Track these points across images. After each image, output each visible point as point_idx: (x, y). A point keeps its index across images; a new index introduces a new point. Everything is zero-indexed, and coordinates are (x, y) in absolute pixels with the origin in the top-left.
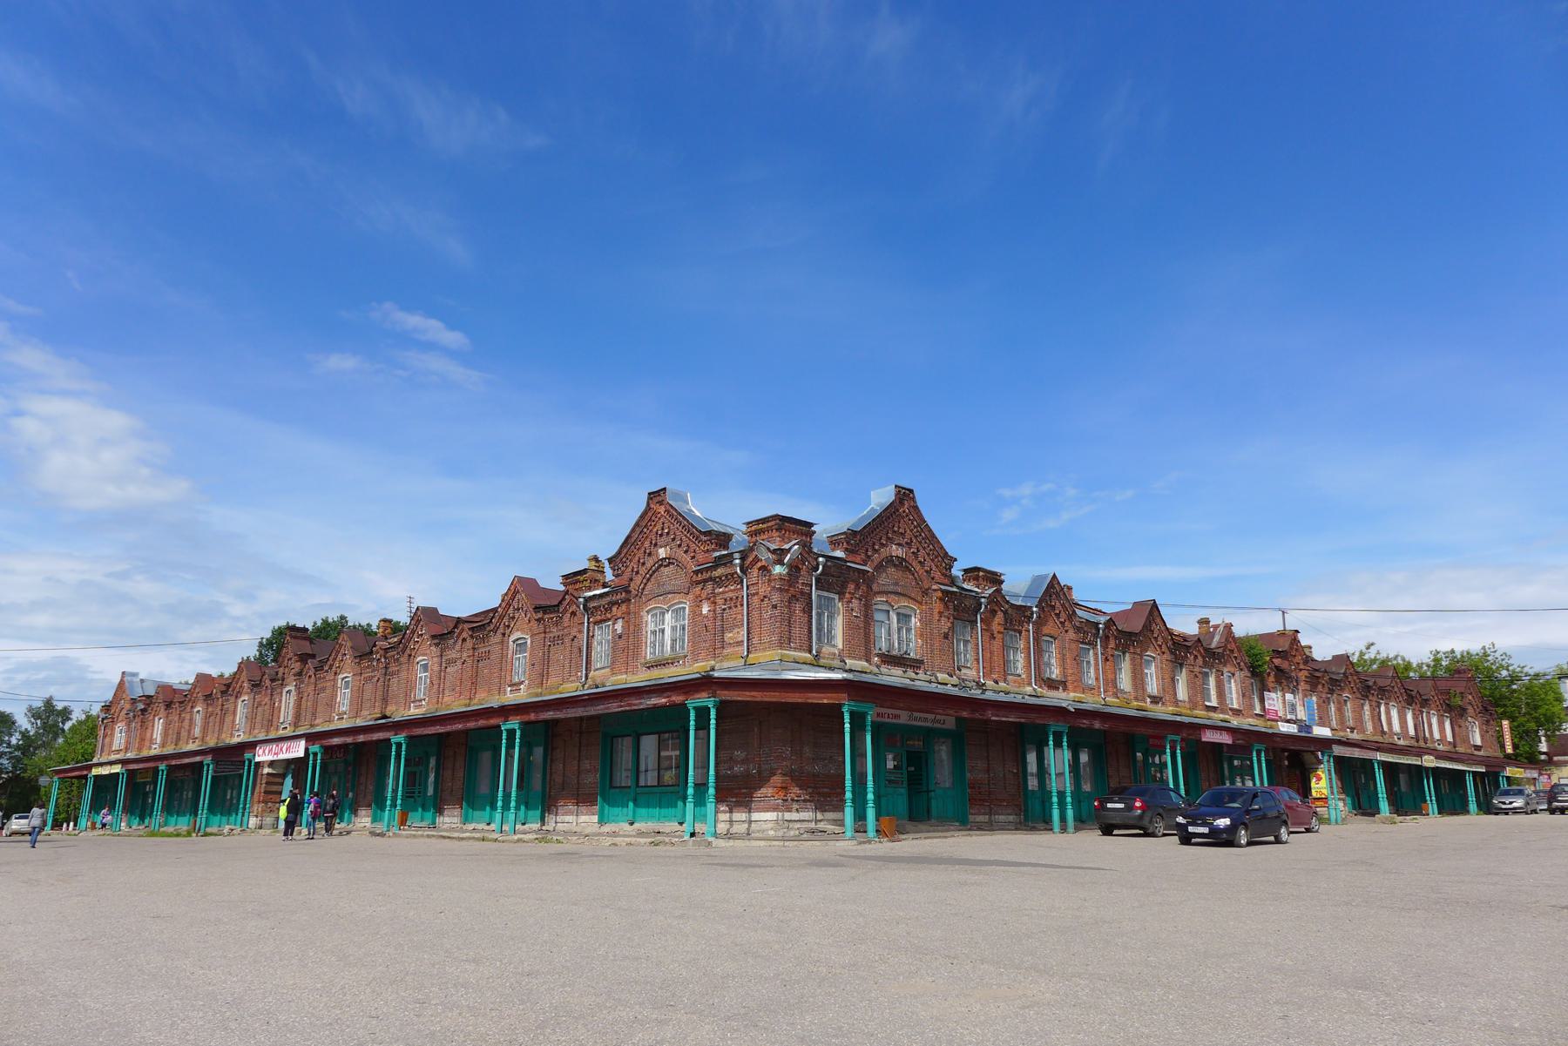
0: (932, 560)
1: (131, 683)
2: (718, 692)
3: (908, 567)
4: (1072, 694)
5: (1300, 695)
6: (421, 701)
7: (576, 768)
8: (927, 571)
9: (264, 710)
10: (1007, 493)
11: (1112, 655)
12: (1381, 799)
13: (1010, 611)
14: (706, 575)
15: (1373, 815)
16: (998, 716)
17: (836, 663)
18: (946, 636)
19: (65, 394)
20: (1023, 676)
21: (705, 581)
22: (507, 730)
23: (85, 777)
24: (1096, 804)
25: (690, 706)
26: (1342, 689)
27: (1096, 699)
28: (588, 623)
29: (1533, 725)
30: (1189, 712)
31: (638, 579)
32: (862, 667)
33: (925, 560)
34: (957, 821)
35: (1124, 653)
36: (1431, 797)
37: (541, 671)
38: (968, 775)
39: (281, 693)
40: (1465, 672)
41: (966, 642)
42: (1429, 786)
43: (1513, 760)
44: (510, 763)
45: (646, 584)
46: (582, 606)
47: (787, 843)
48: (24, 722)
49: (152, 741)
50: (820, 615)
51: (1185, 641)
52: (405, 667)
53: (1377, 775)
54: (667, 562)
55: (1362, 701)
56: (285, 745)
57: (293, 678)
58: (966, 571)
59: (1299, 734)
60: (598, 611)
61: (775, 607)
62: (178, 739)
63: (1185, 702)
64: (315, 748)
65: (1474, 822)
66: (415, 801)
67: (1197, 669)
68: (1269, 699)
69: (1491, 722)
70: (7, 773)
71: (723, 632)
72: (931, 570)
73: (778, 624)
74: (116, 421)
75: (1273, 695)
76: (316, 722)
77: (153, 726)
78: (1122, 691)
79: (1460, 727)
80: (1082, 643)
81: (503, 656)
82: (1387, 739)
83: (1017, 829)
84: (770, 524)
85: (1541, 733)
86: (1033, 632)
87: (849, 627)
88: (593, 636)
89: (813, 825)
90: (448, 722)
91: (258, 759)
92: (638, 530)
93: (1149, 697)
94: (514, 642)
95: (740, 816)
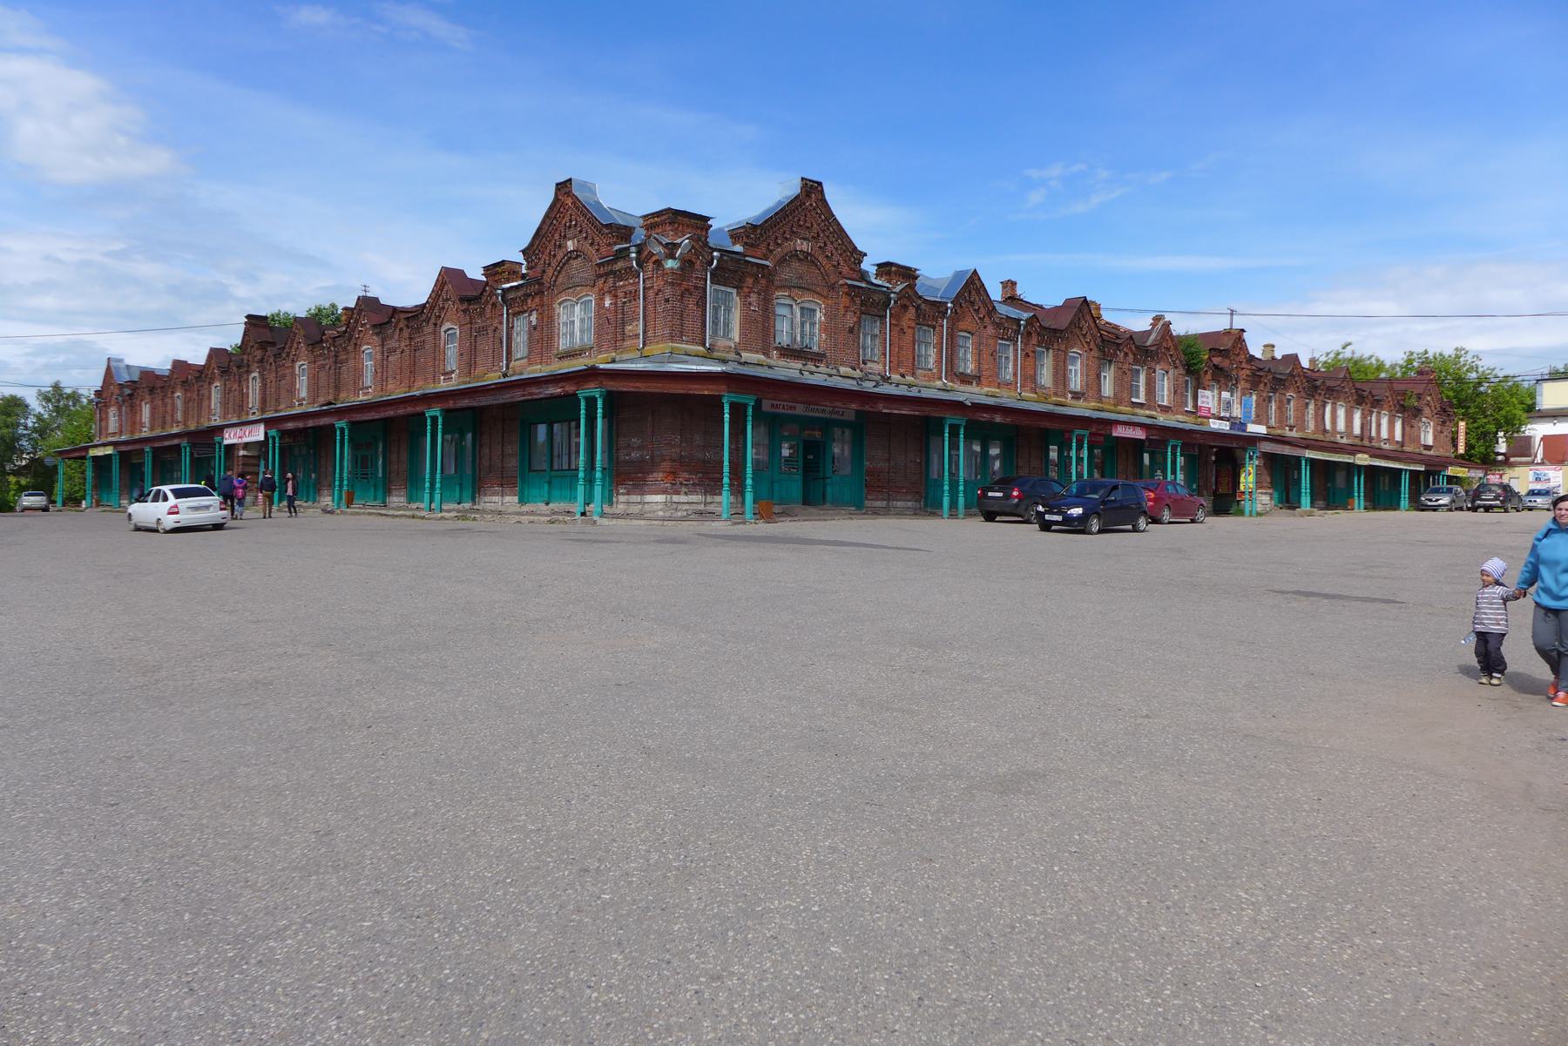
0: (841, 255)
1: (117, 368)
2: (604, 383)
3: (813, 262)
4: (986, 389)
5: (1239, 393)
6: (367, 388)
7: (500, 453)
8: (834, 266)
9: (234, 396)
10: (1034, 173)
11: (1034, 352)
12: (1303, 494)
13: (923, 306)
14: (607, 269)
15: (1294, 508)
16: (890, 409)
17: (732, 356)
18: (851, 331)
19: (21, 51)
20: (935, 371)
21: (606, 275)
22: (431, 417)
23: (84, 458)
24: (979, 492)
25: (580, 396)
26: (1286, 388)
27: (1012, 394)
28: (508, 314)
29: (1492, 428)
30: (1112, 408)
31: (550, 272)
32: (759, 360)
33: (832, 255)
34: (852, 506)
35: (1048, 349)
36: (1359, 493)
37: (470, 359)
38: (867, 463)
39: (248, 379)
40: (1427, 374)
41: (874, 337)
42: (1359, 484)
43: (1466, 460)
44: (435, 446)
45: (557, 277)
46: (500, 298)
47: (666, 523)
48: (36, 405)
49: (142, 425)
50: (716, 310)
51: (1118, 338)
52: (352, 355)
53: (1303, 472)
54: (577, 254)
55: (1307, 401)
56: (247, 429)
57: (256, 365)
58: (879, 266)
59: (1233, 432)
60: (516, 303)
61: (667, 301)
62: (164, 423)
63: (1110, 398)
64: (273, 432)
65: (1404, 516)
66: (368, 482)
67: (1126, 366)
68: (1202, 397)
69: (1448, 423)
70: (28, 454)
71: (623, 324)
72: (839, 264)
73: (669, 318)
74: (82, 83)
75: (1208, 393)
76: (280, 408)
77: (141, 410)
78: (1043, 387)
79: (1412, 427)
80: (1002, 339)
81: (436, 346)
82: (1329, 438)
83: (915, 514)
84: (663, 218)
85: (1501, 434)
86: (948, 328)
87: (747, 321)
88: (513, 327)
89: (702, 507)
90: (382, 409)
91: (226, 442)
92: (548, 222)
93: (1071, 392)
94: (445, 332)
95: (635, 498)
